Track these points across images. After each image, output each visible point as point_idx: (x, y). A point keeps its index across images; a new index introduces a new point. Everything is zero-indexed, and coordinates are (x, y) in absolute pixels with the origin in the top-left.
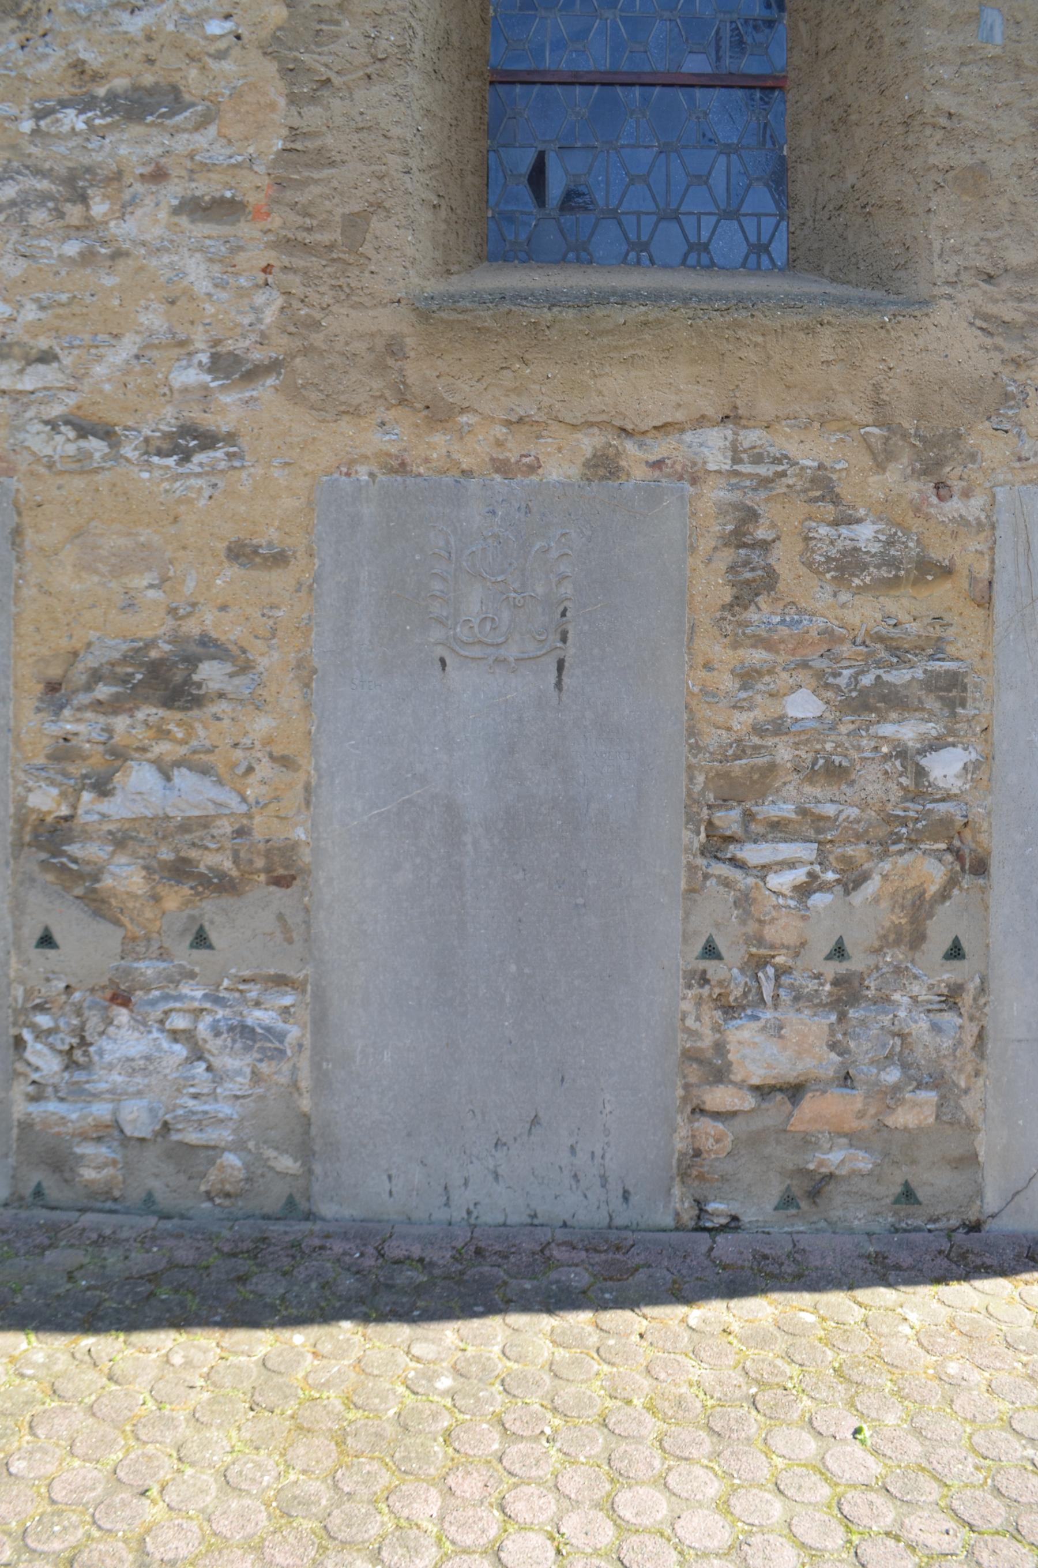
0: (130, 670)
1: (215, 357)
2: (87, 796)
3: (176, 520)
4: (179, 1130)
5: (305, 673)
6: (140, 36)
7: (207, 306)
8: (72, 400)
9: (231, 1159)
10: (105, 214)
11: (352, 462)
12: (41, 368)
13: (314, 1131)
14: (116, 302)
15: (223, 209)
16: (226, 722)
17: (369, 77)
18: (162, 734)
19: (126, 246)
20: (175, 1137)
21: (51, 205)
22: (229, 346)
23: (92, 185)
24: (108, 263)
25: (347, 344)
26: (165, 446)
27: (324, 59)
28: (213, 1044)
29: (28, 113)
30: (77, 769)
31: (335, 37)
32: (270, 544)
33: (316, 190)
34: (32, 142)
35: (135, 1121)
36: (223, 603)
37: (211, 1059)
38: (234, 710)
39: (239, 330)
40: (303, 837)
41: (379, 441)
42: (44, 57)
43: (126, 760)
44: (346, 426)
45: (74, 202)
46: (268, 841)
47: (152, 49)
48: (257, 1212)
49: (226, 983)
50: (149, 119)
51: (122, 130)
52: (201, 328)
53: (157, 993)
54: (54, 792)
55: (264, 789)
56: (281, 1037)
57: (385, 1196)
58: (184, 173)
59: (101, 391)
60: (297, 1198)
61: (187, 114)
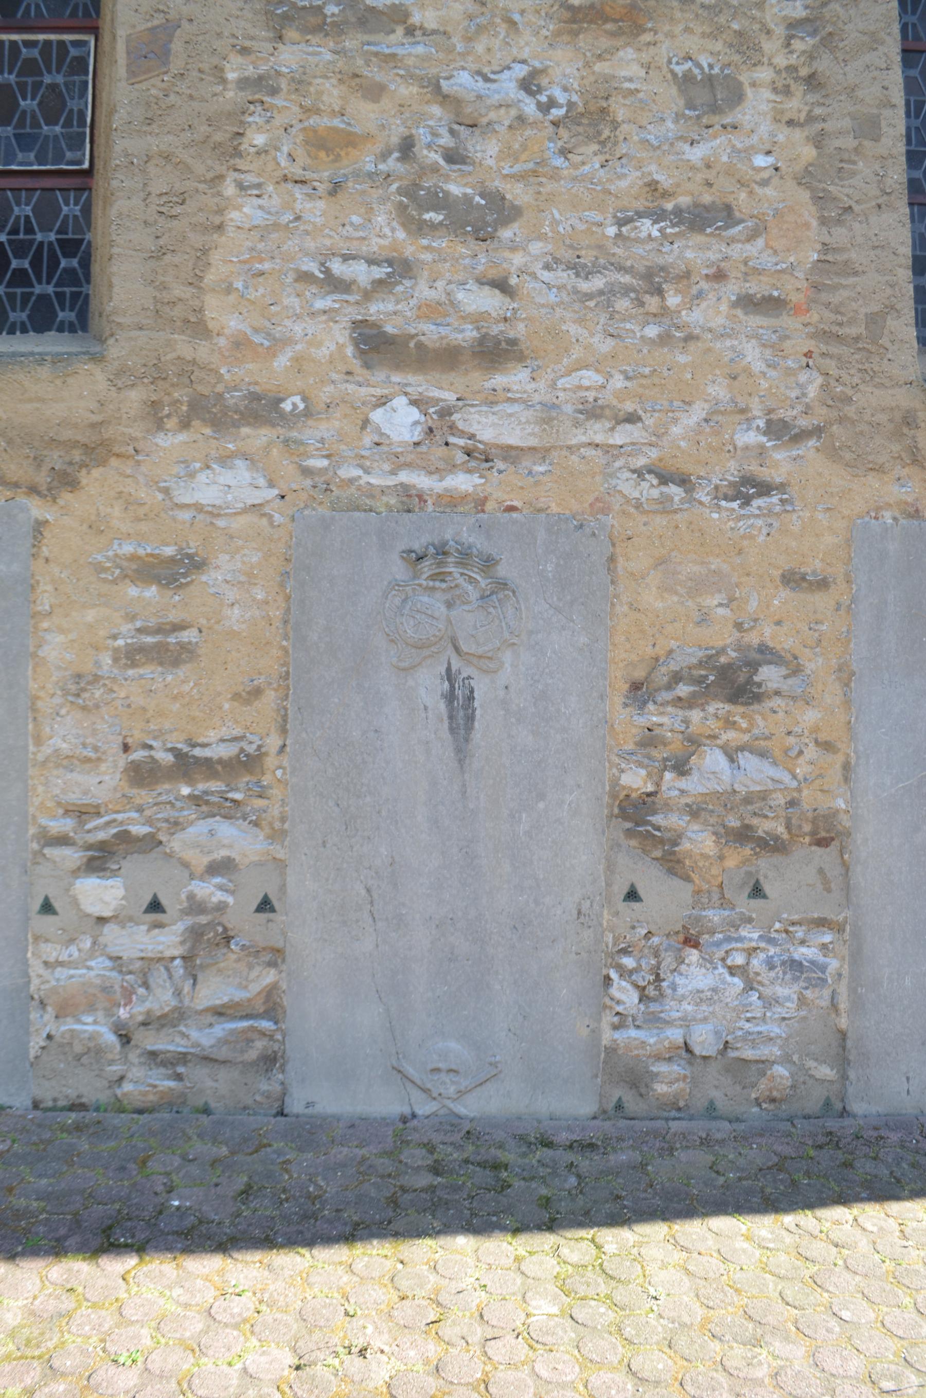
0: (703, 673)
1: (769, 422)
2: (668, 776)
3: (740, 552)
4: (737, 1049)
5: (845, 675)
6: (699, 164)
7: (762, 382)
8: (654, 453)
9: (780, 1070)
10: (678, 305)
11: (878, 509)
12: (628, 426)
13: (849, 1044)
14: (689, 376)
15: (769, 305)
16: (781, 714)
17: (879, 206)
18: (729, 724)
19: (697, 331)
20: (732, 1054)
21: (632, 295)
22: (781, 414)
23: (666, 281)
24: (681, 345)
25: (873, 415)
26: (730, 493)
27: (846, 191)
28: (766, 976)
29: (610, 220)
30: (659, 754)
31: (854, 174)
32: (814, 573)
33: (845, 293)
34: (615, 244)
35: (703, 1042)
36: (779, 620)
37: (761, 988)
38: (787, 705)
39: (788, 402)
40: (843, 806)
41: (897, 493)
42: (623, 176)
43: (700, 746)
44: (873, 480)
45: (652, 294)
46: (815, 810)
47: (711, 175)
48: (799, 1113)
49: (777, 926)
50: (709, 230)
51: (687, 238)
52: (757, 399)
53: (721, 936)
54: (643, 772)
55: (809, 769)
56: (823, 968)
57: (904, 1094)
58: (739, 275)
59: (679, 447)
60: (833, 1099)
61: (740, 227)
